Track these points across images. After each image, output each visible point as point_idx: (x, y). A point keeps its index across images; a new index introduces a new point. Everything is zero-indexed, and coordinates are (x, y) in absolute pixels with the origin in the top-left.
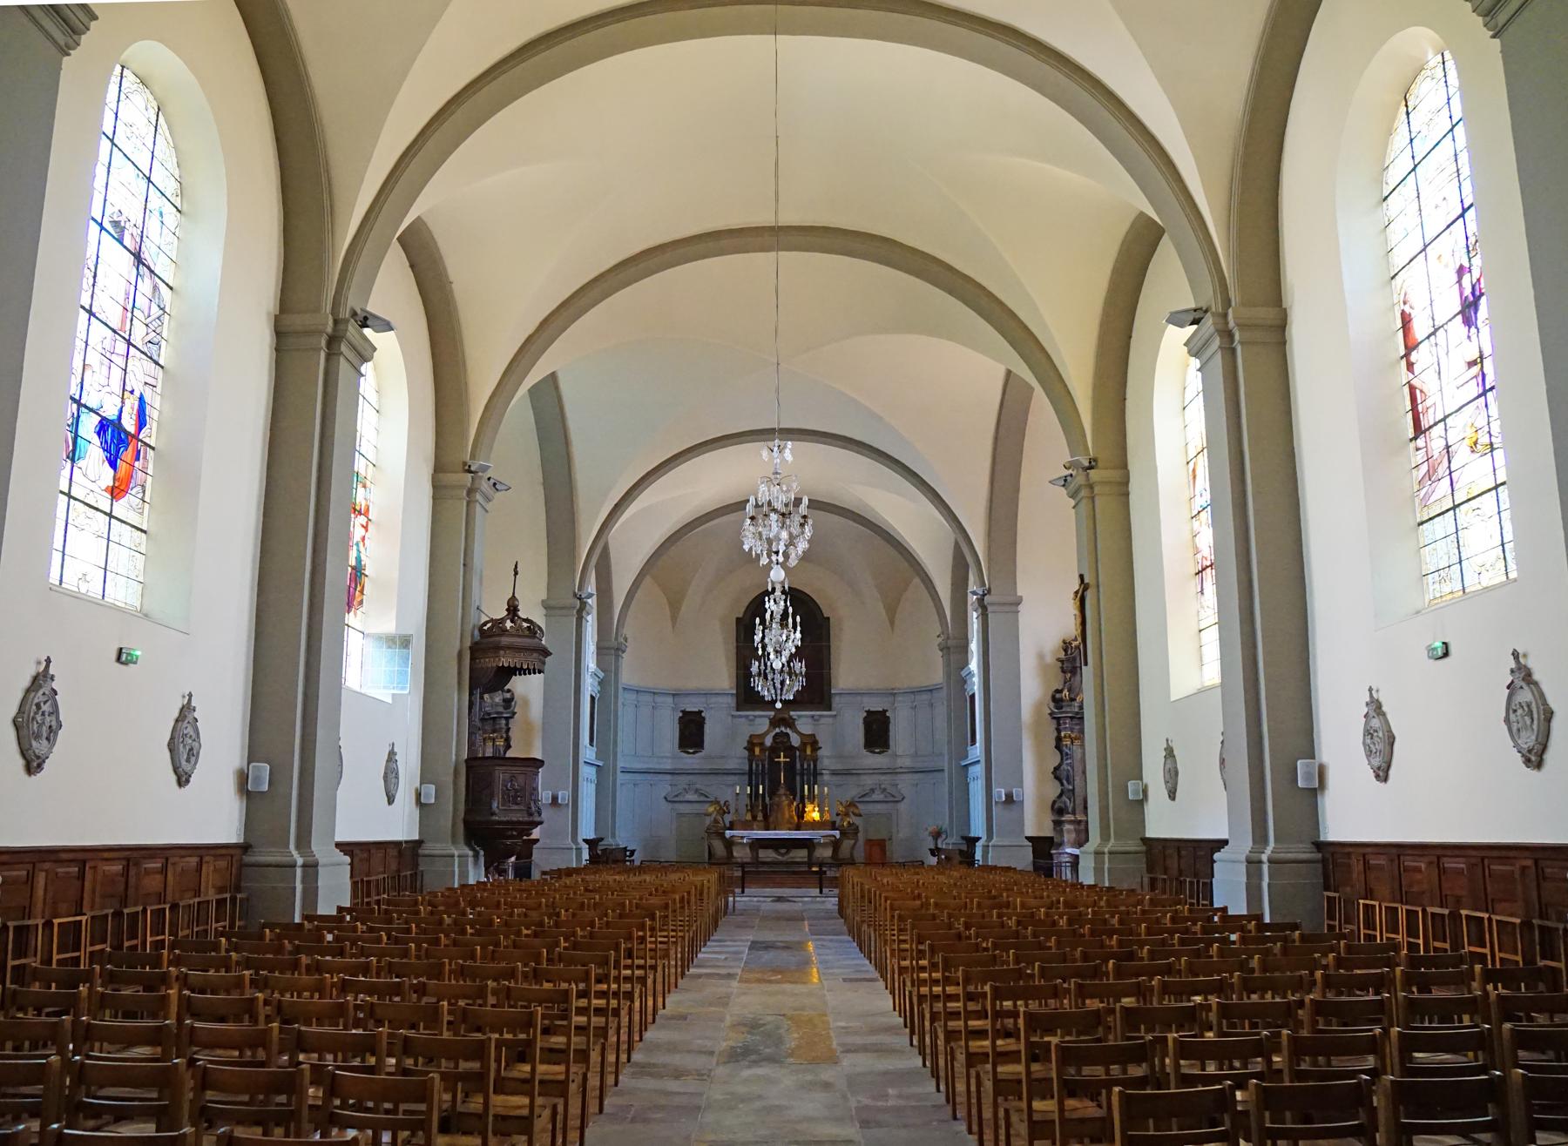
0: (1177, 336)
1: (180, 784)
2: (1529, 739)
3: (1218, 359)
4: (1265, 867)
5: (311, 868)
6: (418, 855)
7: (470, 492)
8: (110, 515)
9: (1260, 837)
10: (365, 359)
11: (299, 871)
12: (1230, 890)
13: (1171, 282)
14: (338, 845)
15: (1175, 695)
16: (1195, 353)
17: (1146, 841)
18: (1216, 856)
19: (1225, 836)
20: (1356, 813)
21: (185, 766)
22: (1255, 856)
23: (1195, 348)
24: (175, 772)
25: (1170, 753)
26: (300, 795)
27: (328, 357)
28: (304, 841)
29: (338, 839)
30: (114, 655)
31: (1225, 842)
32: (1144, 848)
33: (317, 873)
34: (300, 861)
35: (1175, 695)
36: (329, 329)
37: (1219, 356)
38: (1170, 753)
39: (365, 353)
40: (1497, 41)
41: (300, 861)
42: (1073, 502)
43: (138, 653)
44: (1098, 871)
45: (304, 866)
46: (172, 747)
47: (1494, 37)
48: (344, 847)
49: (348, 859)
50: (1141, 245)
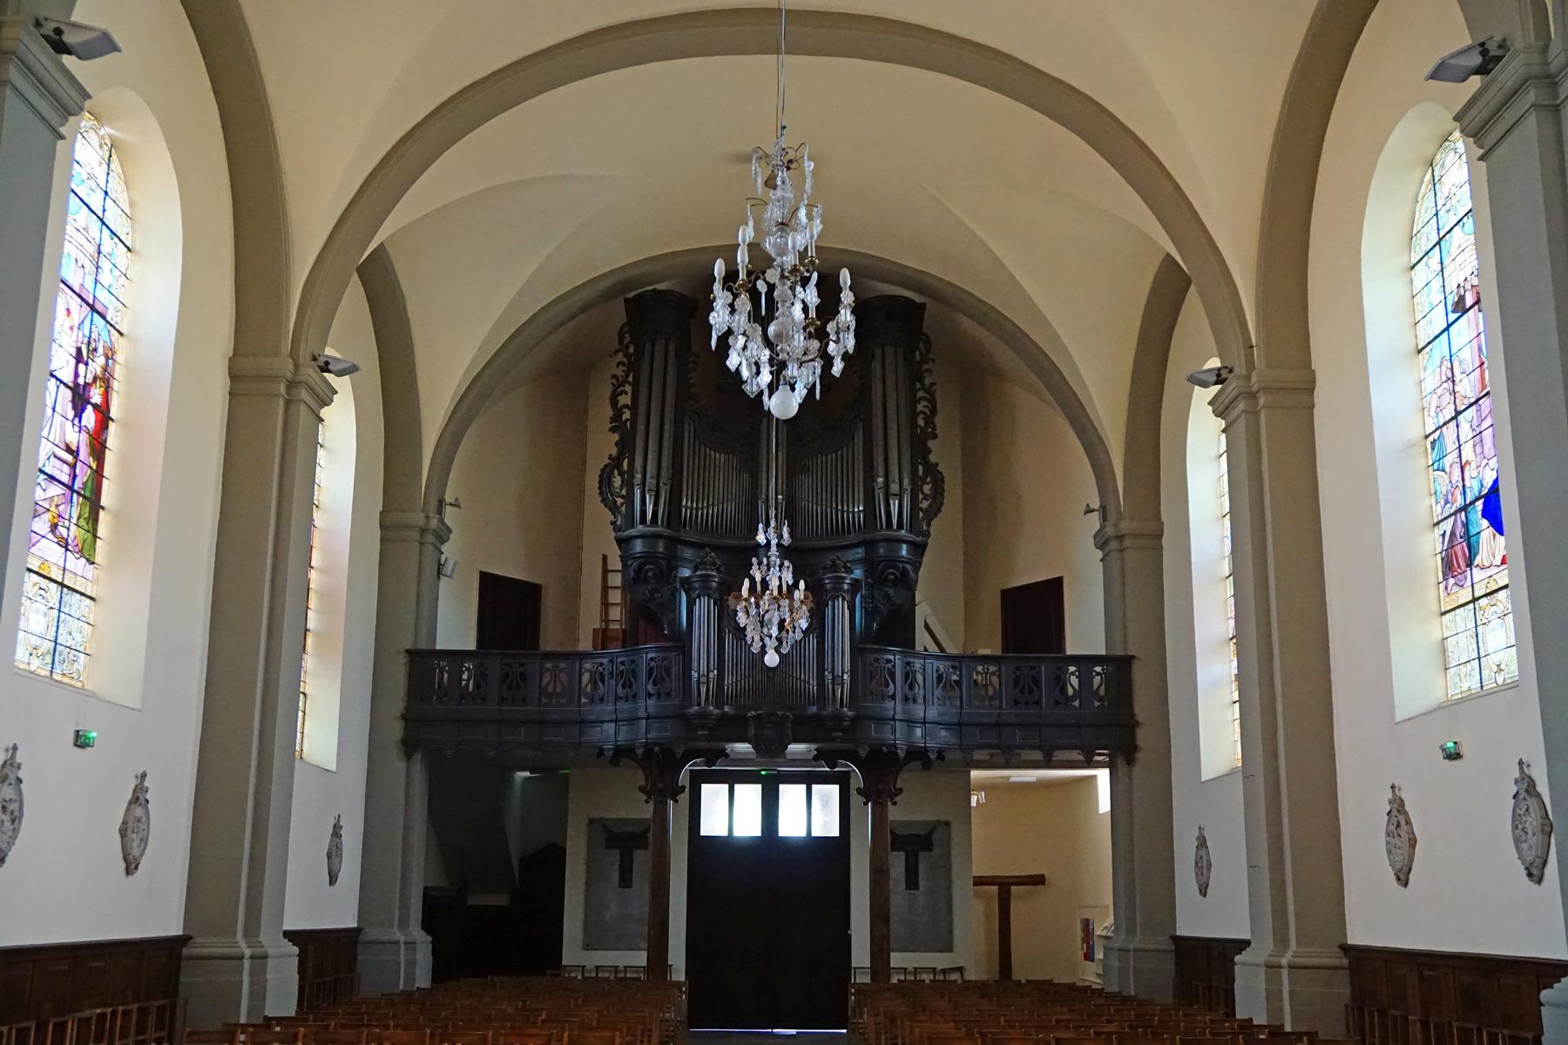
0: (1202, 397)
1: (128, 872)
2: (1400, 856)
3: (1242, 422)
4: (1285, 973)
5: (260, 958)
6: (180, 958)
7: (292, 385)
8: (62, 585)
9: (1281, 940)
10: (326, 402)
11: (247, 963)
12: (1250, 1004)
13: (1197, 346)
14: (287, 934)
15: (1401, 713)
16: (1219, 413)
17: (1347, 950)
18: (1237, 958)
19: (1247, 936)
20: (1381, 917)
21: (135, 851)
22: (1274, 960)
23: (1220, 408)
24: (125, 859)
25: (1202, 843)
26: (249, 888)
27: (288, 403)
28: (252, 929)
29: (286, 928)
30: (72, 737)
31: (1247, 943)
32: (1345, 962)
33: (265, 965)
34: (248, 952)
35: (1401, 713)
36: (289, 376)
37: (1532, 120)
38: (1202, 843)
39: (325, 397)
40: (1483, 164)
41: (248, 952)
42: (1100, 554)
43: (94, 734)
44: (1273, 995)
45: (252, 957)
46: (123, 833)
47: (1481, 158)
48: (290, 935)
49: (296, 950)
50: (1170, 290)
